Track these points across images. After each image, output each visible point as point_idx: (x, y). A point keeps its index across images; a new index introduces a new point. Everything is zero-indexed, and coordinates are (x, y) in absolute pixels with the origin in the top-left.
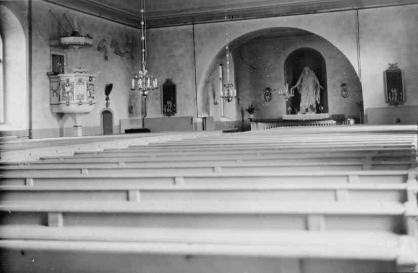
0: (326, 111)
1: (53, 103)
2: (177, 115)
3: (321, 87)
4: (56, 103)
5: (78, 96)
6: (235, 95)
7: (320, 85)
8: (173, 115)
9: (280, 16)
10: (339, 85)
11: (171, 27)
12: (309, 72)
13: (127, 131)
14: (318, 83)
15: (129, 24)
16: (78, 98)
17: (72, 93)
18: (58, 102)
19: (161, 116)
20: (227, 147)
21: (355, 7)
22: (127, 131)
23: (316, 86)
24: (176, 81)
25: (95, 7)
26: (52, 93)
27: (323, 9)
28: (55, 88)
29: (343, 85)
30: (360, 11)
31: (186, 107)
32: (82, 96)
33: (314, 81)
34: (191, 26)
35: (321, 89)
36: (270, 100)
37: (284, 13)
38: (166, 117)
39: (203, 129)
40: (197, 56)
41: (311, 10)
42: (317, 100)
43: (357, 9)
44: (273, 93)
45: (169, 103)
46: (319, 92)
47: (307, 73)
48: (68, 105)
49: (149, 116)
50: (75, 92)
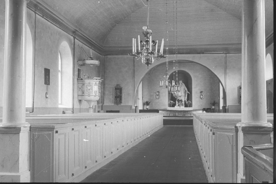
0: (191, 105)
1: (79, 94)
2: (122, 104)
3: (188, 92)
4: (81, 94)
5: (95, 91)
6: (97, 98)
7: (188, 91)
8: (120, 104)
9: (184, 54)
10: (199, 92)
11: (120, 56)
12: (182, 84)
13: (141, 111)
14: (186, 89)
15: (98, 52)
16: (95, 93)
17: (92, 90)
18: (82, 94)
19: (113, 104)
20: (11, 131)
21: (225, 52)
22: (141, 111)
23: (185, 92)
24: (122, 86)
25: (87, 40)
26: (79, 89)
27: (208, 52)
28: (80, 87)
29: (201, 92)
30: (227, 54)
31: (127, 101)
32: (96, 92)
33: (184, 89)
34: (224, 55)
35: (188, 94)
36: (159, 98)
37: (186, 52)
38: (115, 105)
39: (135, 112)
40: (136, 73)
41: (201, 52)
42: (186, 99)
43: (226, 53)
44: (160, 94)
45: (118, 99)
46: (187, 95)
47: (181, 84)
48: (89, 96)
49: (105, 104)
50: (93, 90)
